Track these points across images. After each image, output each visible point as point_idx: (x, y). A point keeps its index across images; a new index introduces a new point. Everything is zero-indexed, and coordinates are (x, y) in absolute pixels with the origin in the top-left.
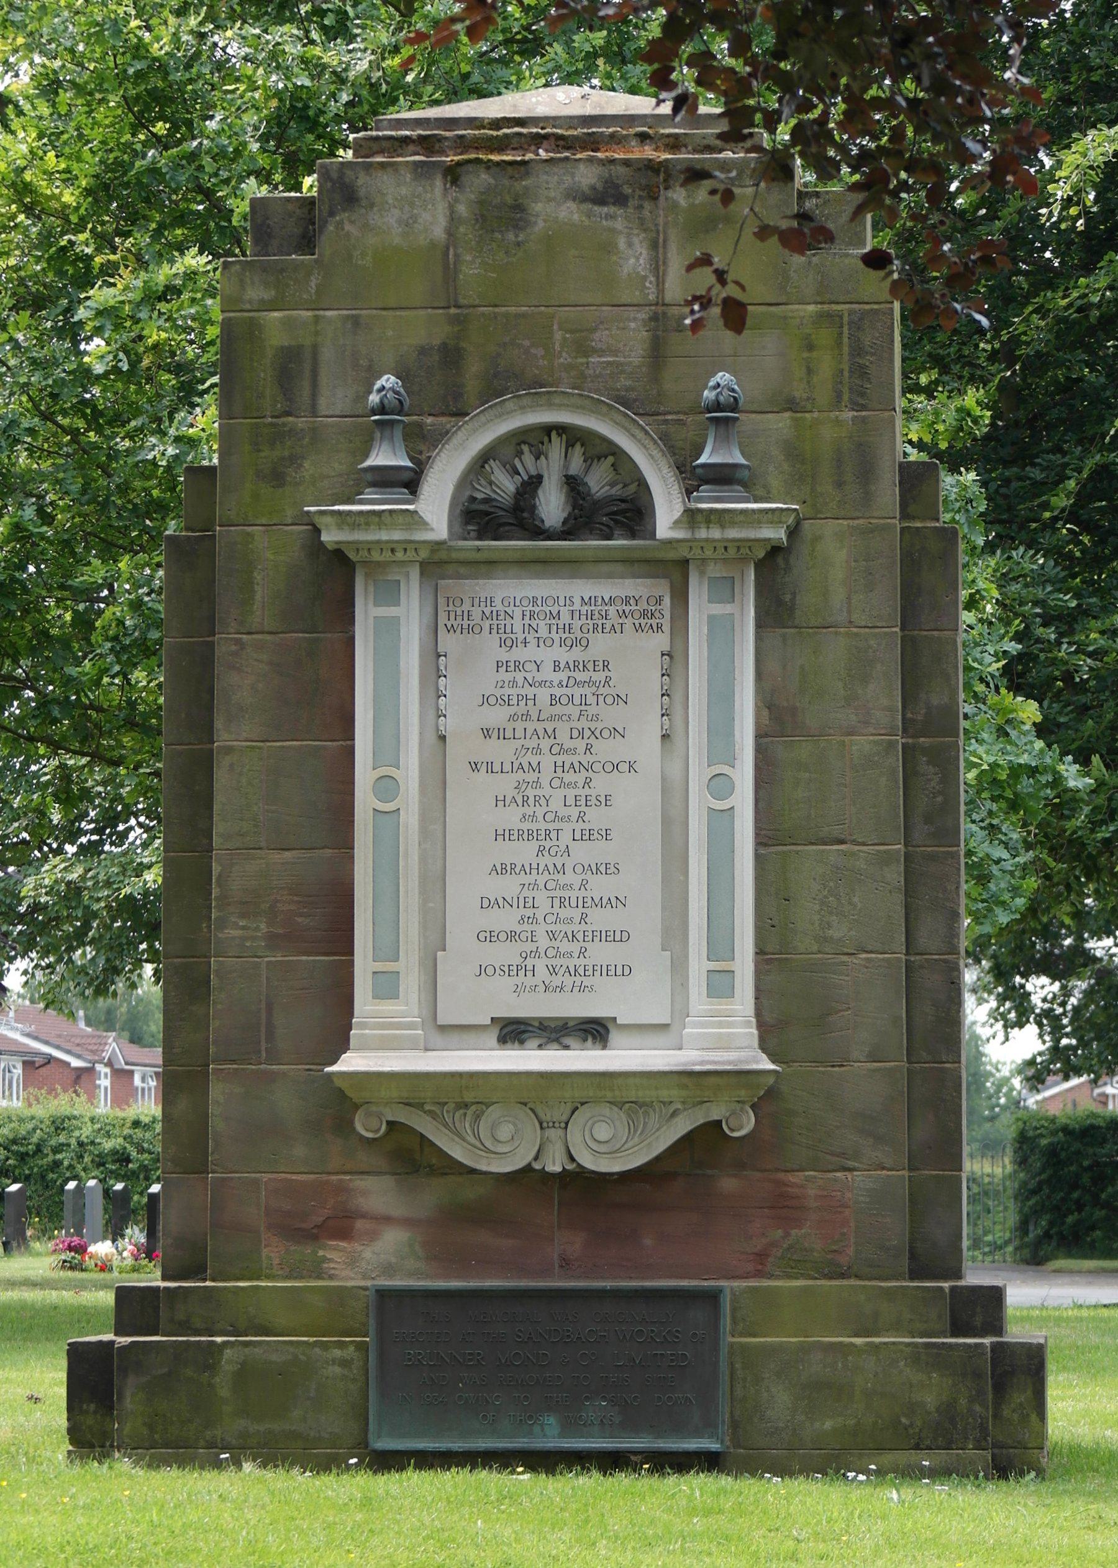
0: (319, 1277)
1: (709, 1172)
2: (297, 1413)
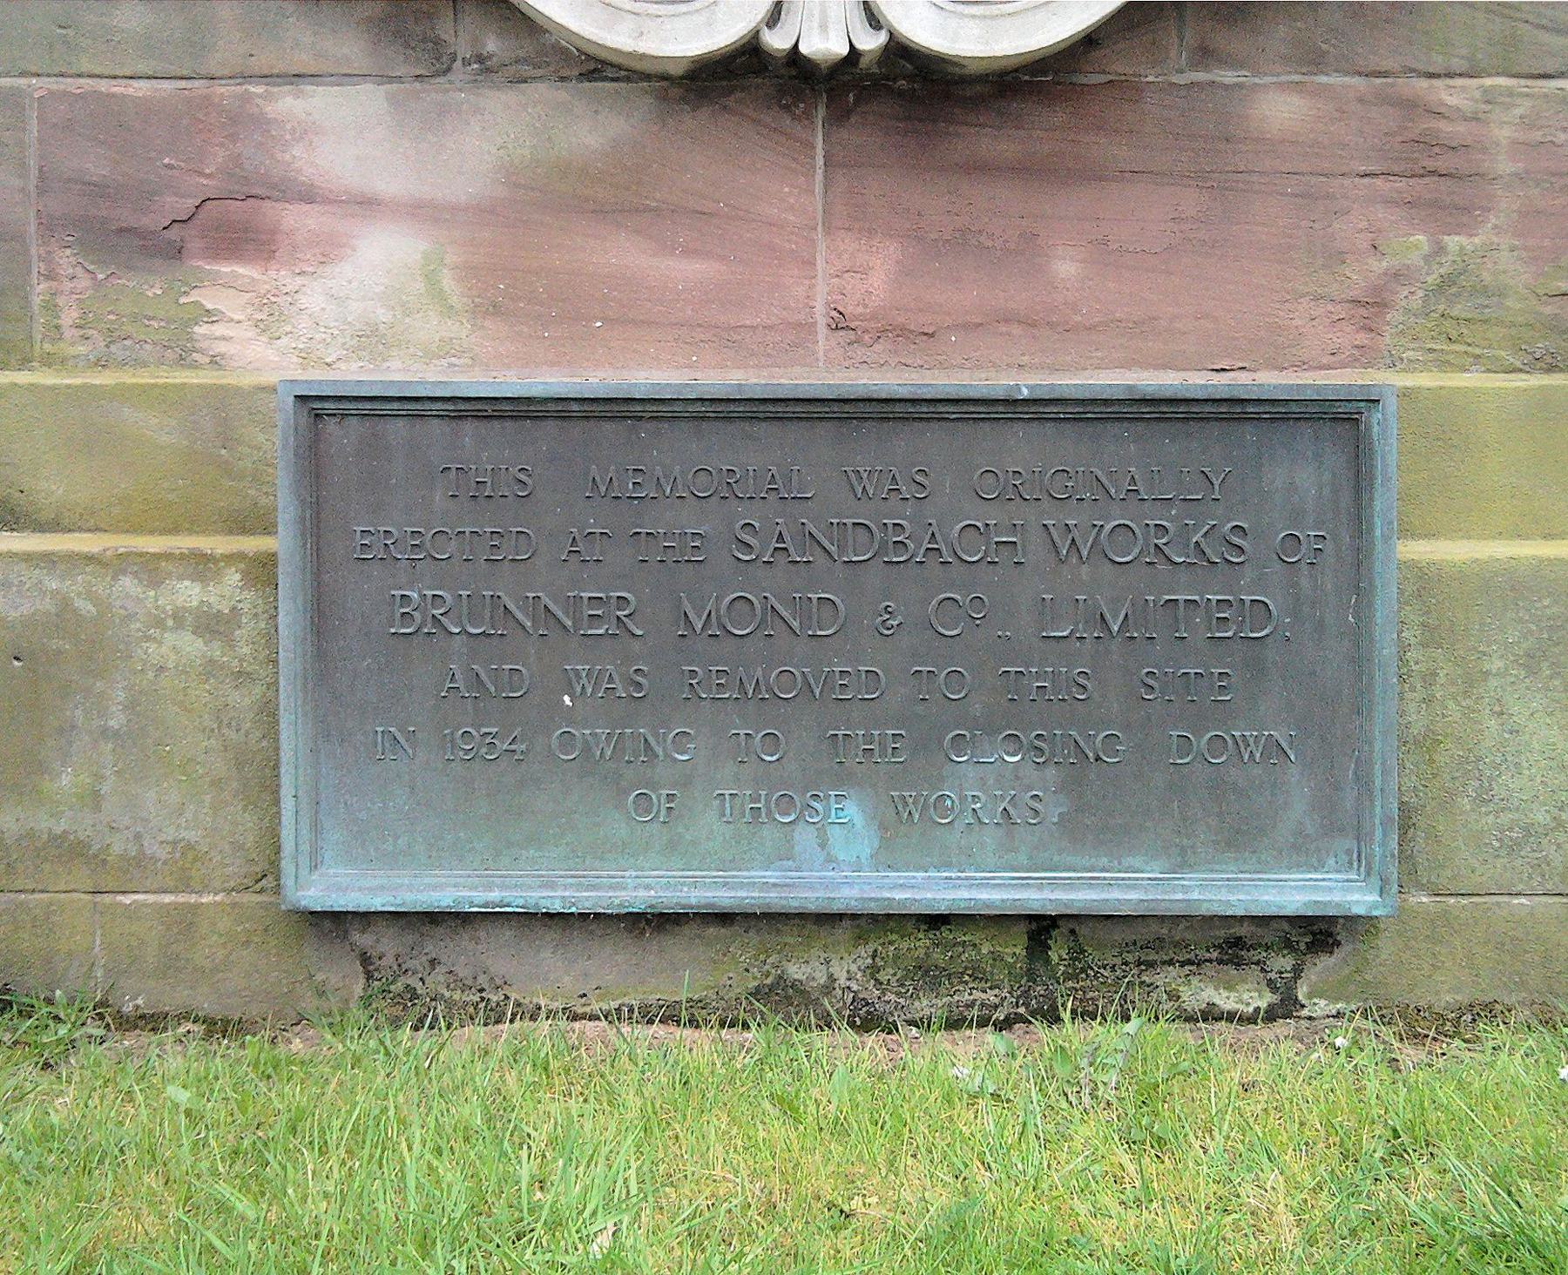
0: (182, 361)
1: (1228, 77)
2: (67, 780)
